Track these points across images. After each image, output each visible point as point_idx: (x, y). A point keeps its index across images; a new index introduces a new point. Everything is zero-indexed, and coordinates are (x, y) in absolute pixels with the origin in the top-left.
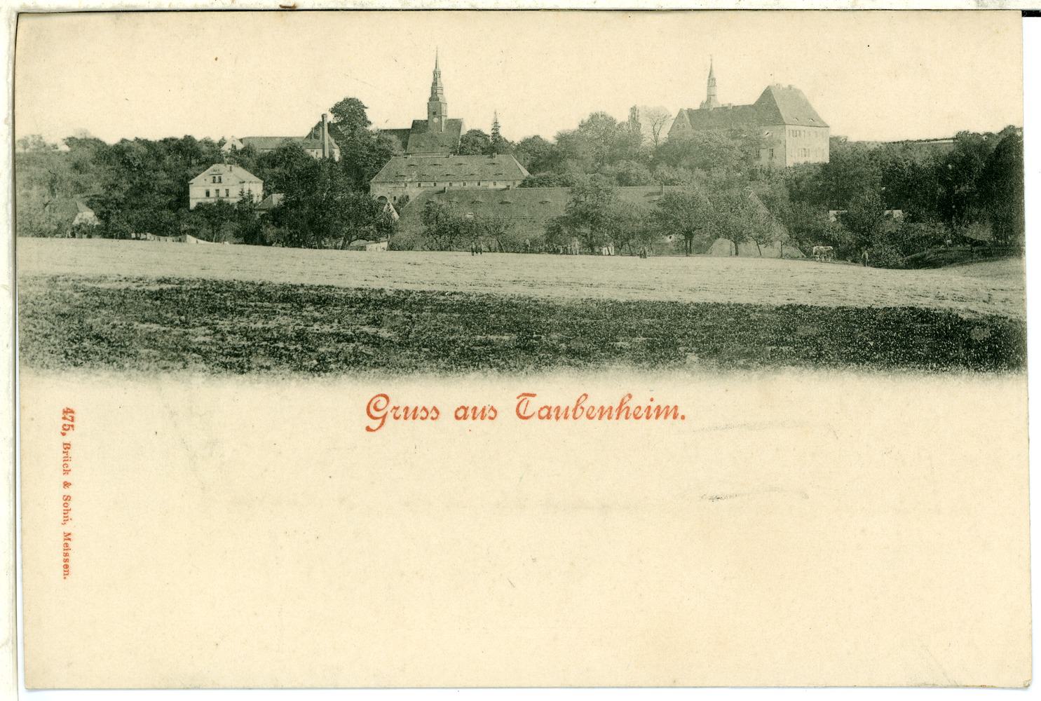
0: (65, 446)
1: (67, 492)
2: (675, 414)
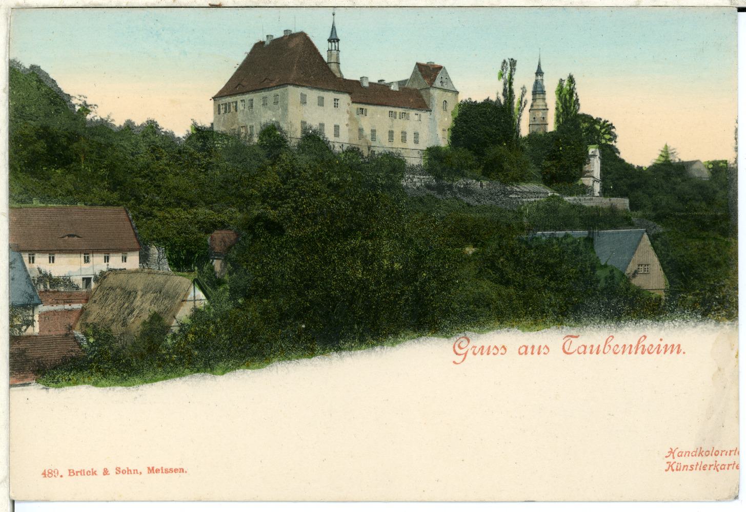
0: (72, 474)
1: (112, 471)
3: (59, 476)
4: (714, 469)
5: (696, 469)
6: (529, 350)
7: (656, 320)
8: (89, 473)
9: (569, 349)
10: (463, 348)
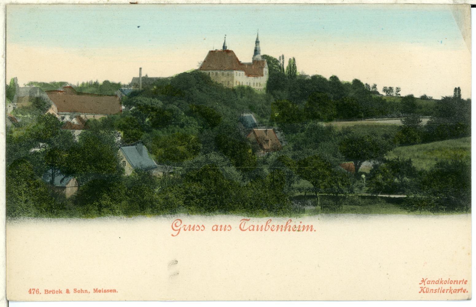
0: (47, 293)
1: (72, 291)
2: (311, 229)
3: (39, 294)
4: (449, 292)
5: (438, 292)
6: (219, 228)
7: (12, 216)
8: (57, 292)
9: (243, 228)
10: (178, 226)
